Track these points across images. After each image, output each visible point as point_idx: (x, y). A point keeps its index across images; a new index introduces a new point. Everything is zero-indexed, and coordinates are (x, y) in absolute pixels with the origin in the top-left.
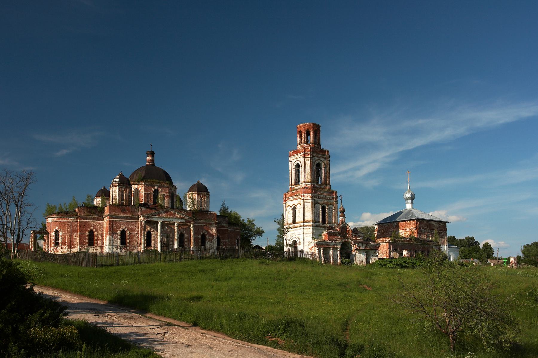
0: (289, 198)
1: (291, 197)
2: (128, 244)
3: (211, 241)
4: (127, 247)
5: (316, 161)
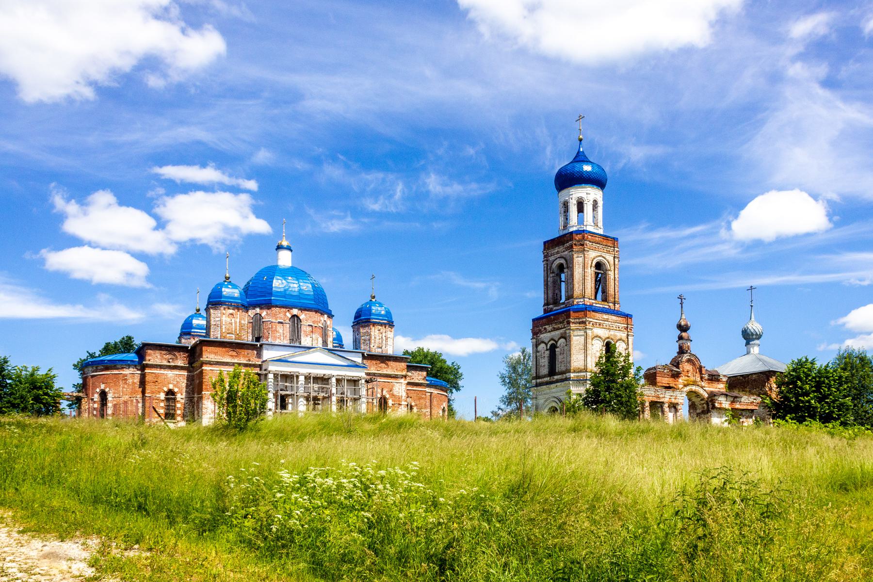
1: (547, 327)
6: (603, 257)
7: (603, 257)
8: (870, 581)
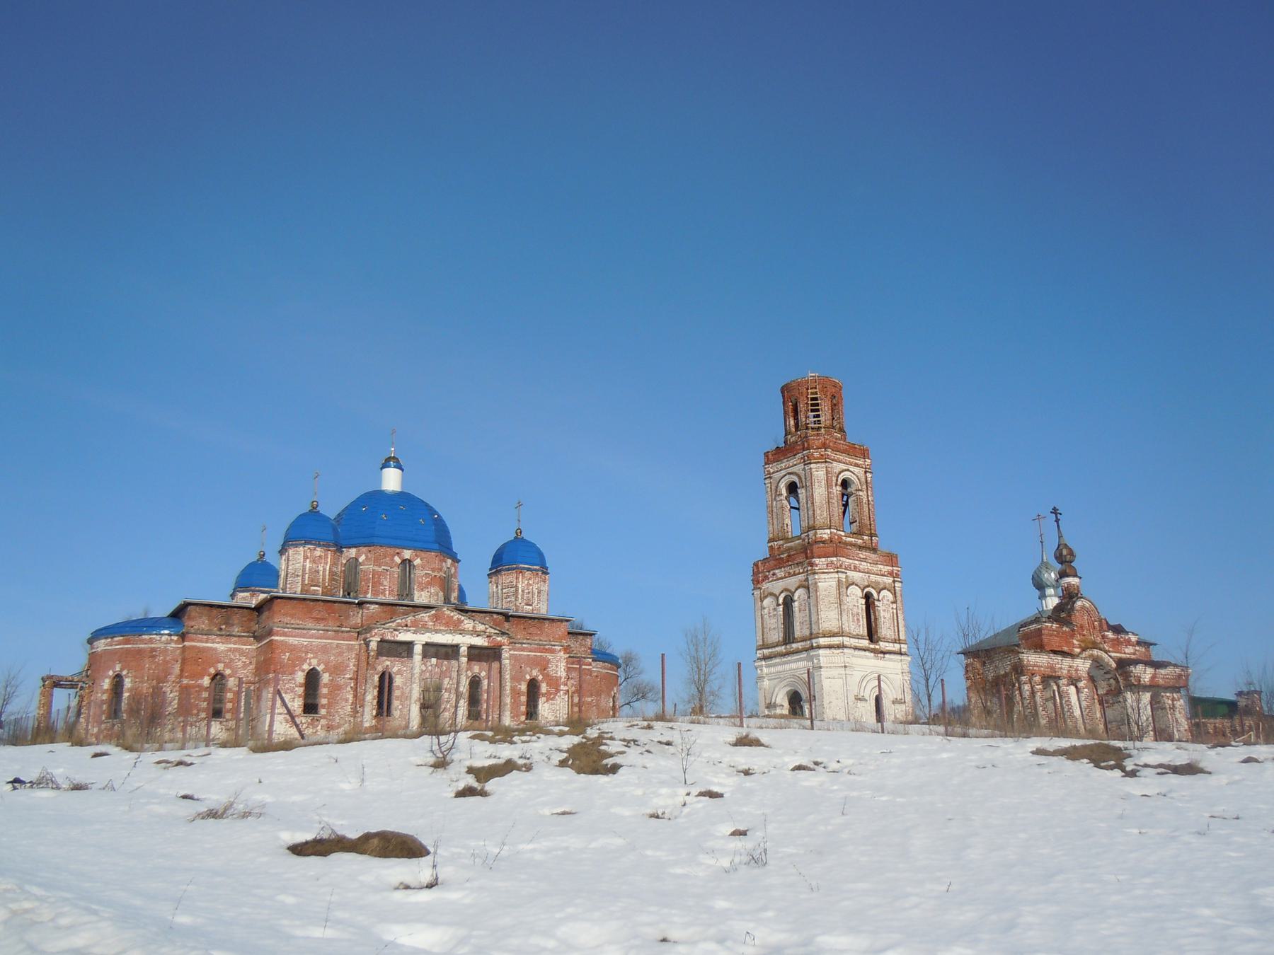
0: (772, 572)
1: (776, 571)
2: (323, 712)
3: (552, 699)
5: (840, 473)
6: (851, 472)
7: (851, 472)
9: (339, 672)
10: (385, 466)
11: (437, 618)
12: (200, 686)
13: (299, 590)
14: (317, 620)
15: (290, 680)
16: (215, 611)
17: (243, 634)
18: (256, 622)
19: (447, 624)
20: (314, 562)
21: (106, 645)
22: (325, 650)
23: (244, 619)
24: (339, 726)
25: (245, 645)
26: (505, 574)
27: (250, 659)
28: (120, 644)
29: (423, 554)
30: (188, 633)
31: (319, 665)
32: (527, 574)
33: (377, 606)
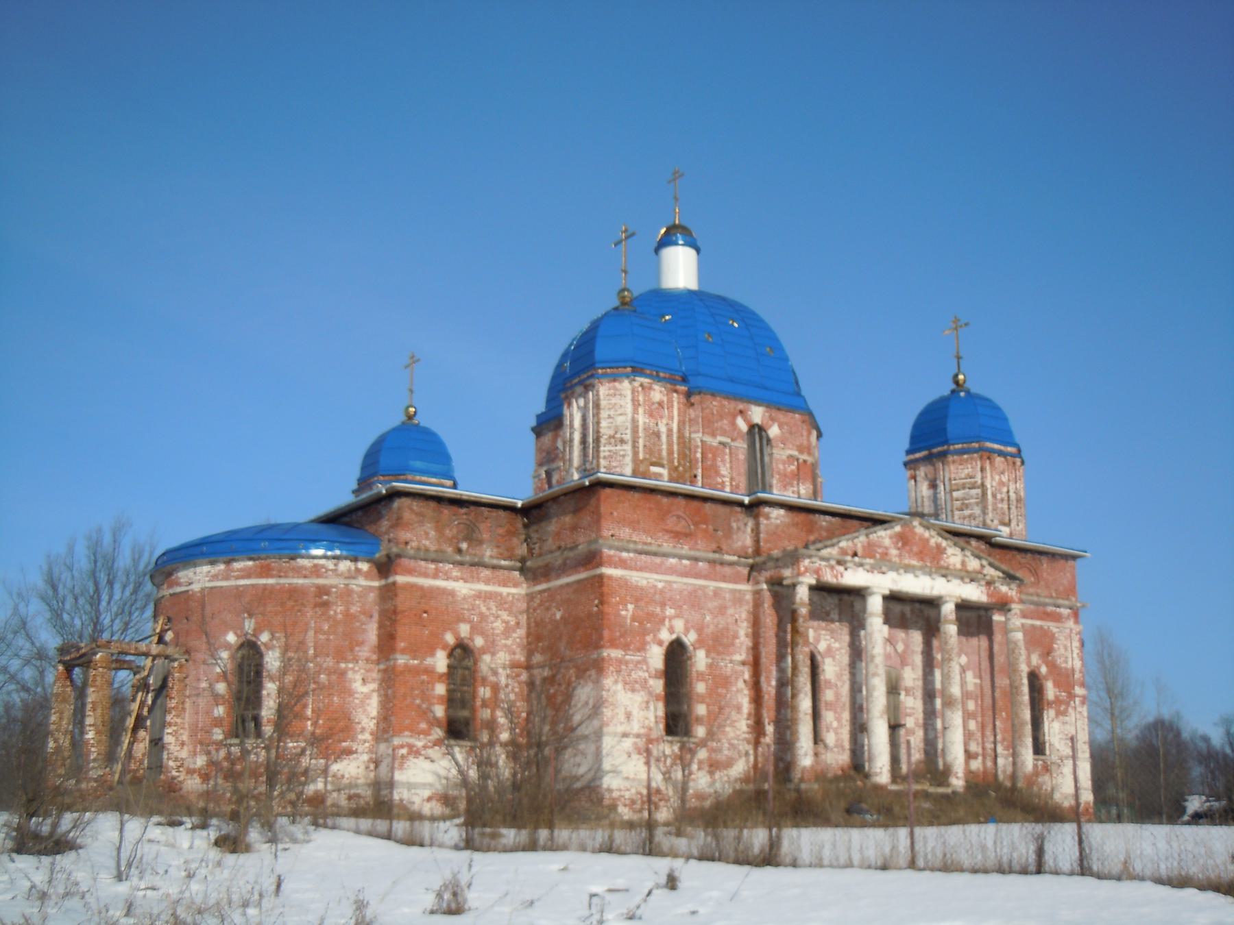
2: (700, 731)
4: (697, 745)
8: (142, 924)
9: (721, 649)
10: (666, 241)
11: (904, 540)
12: (430, 671)
13: (628, 470)
14: (678, 536)
15: (638, 662)
16: (447, 511)
17: (503, 563)
18: (523, 537)
19: (921, 555)
20: (651, 414)
21: (215, 577)
22: (694, 600)
23: (501, 531)
24: (729, 764)
25: (505, 585)
26: (954, 462)
27: (516, 617)
28: (248, 576)
29: (782, 416)
30: (399, 556)
31: (687, 631)
32: (999, 460)
33: (782, 512)
